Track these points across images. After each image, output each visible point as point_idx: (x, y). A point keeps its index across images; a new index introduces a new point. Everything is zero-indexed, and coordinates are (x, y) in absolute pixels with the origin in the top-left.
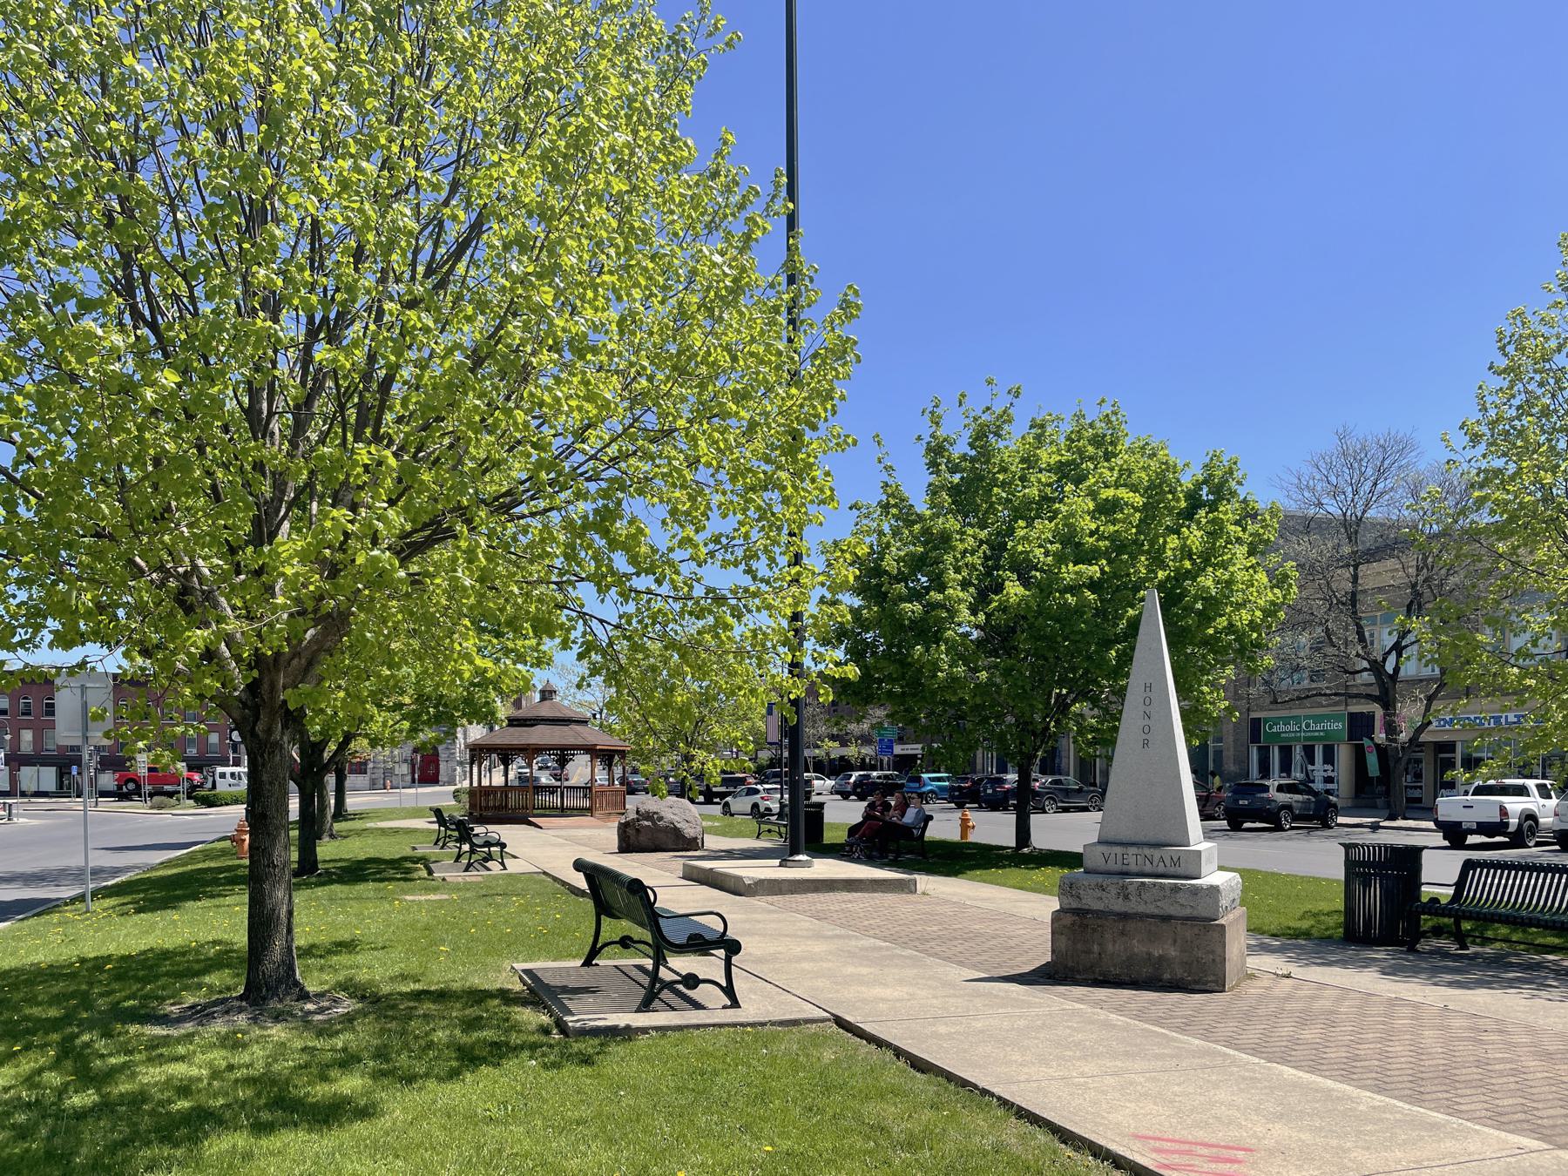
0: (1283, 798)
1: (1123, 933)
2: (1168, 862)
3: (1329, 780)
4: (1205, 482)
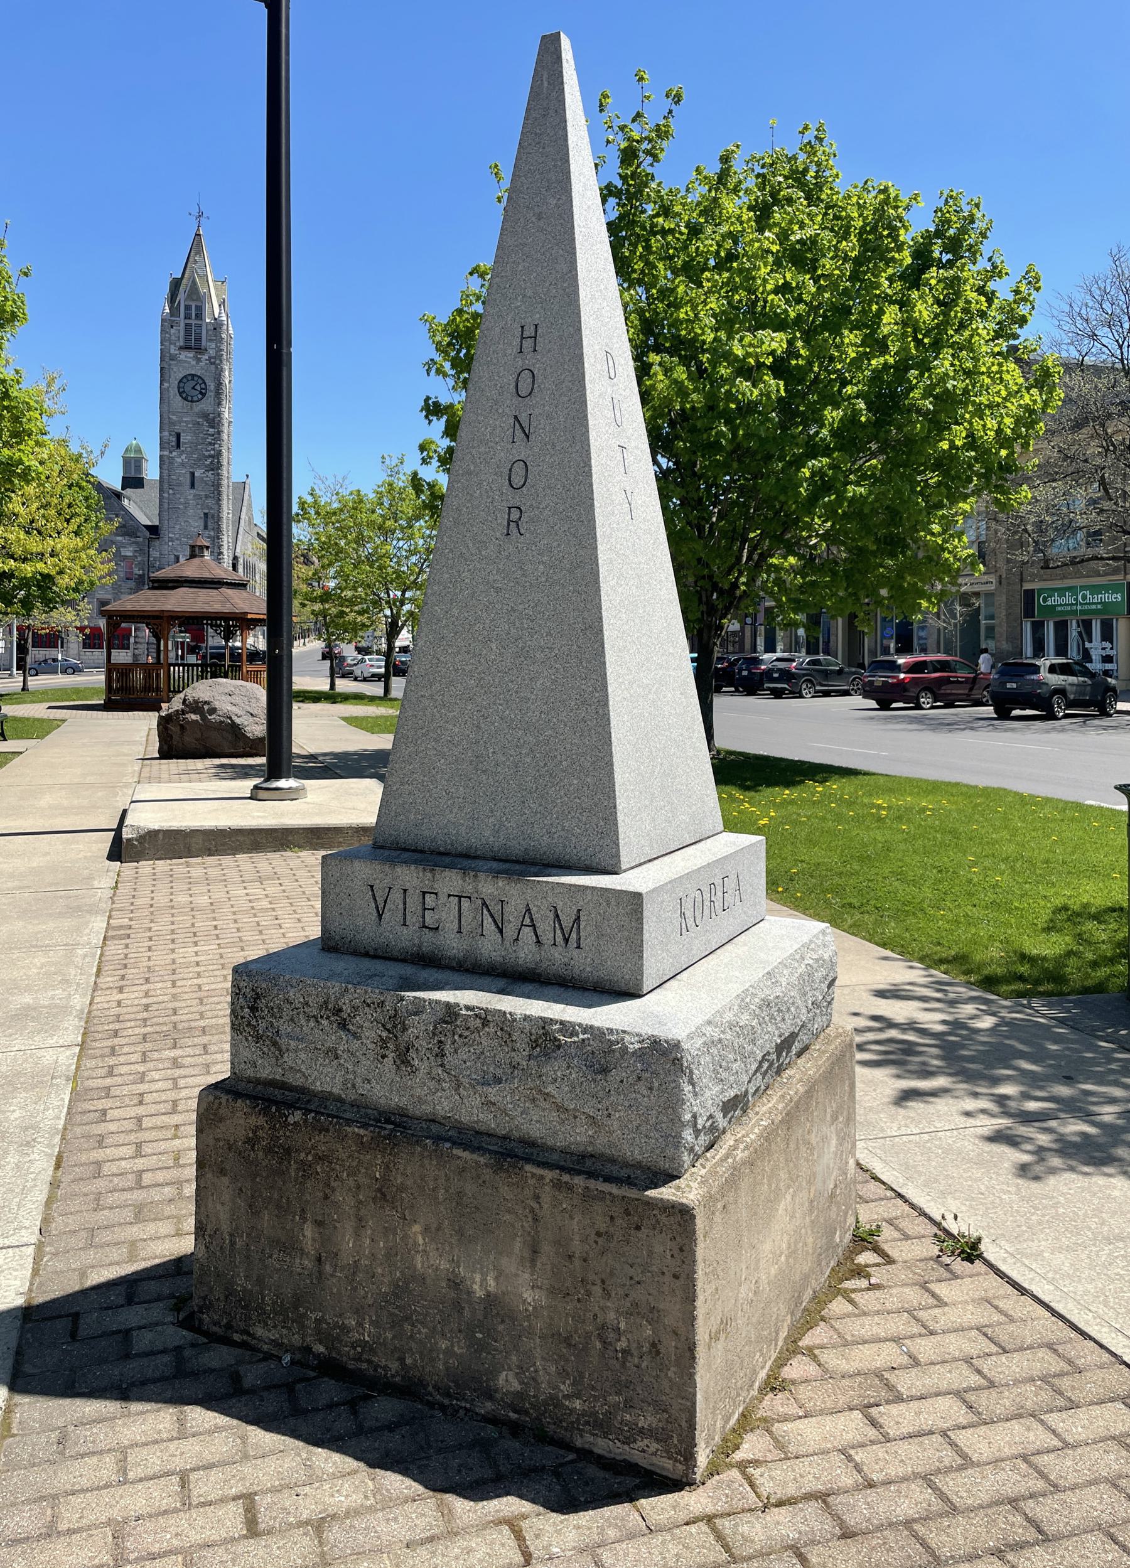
0: (1056, 680)
1: (383, 1195)
2: (545, 927)
3: (1107, 659)
4: (939, 234)
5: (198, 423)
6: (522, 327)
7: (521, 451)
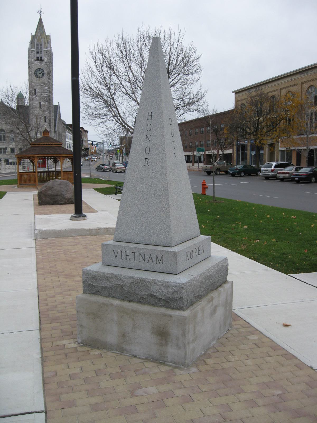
2: (154, 259)
5: (42, 85)
6: (148, 113)
7: (148, 144)
